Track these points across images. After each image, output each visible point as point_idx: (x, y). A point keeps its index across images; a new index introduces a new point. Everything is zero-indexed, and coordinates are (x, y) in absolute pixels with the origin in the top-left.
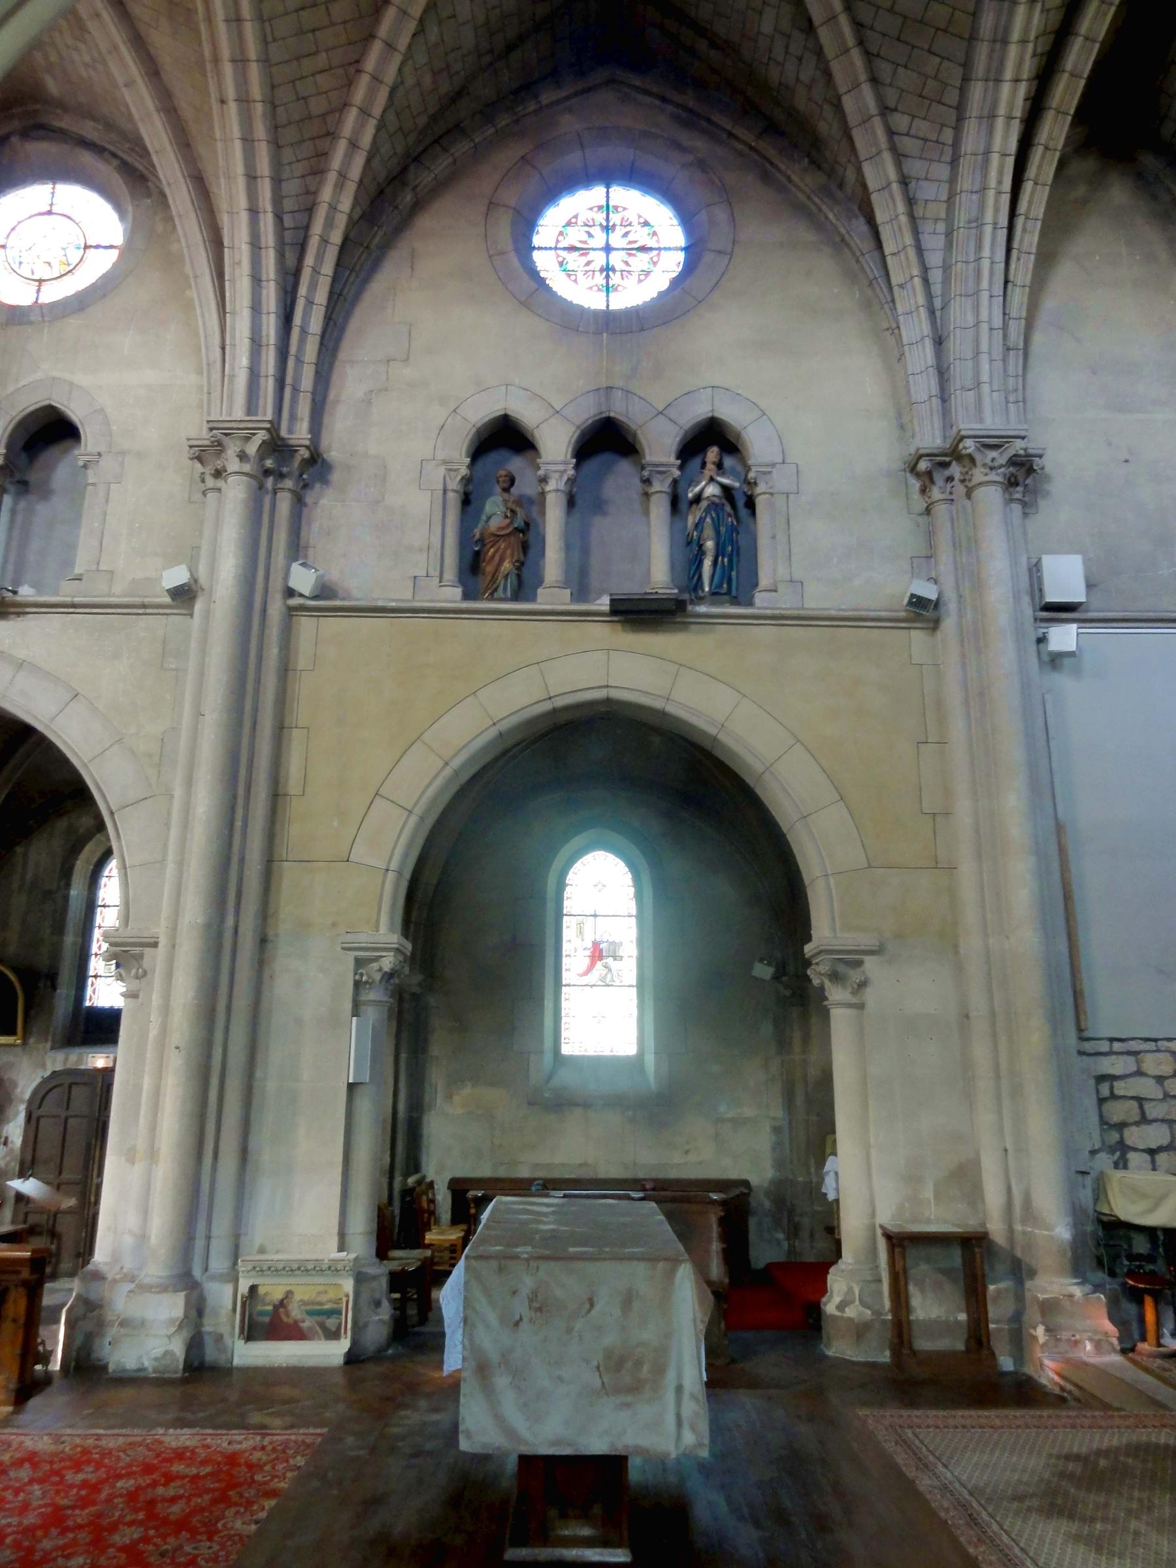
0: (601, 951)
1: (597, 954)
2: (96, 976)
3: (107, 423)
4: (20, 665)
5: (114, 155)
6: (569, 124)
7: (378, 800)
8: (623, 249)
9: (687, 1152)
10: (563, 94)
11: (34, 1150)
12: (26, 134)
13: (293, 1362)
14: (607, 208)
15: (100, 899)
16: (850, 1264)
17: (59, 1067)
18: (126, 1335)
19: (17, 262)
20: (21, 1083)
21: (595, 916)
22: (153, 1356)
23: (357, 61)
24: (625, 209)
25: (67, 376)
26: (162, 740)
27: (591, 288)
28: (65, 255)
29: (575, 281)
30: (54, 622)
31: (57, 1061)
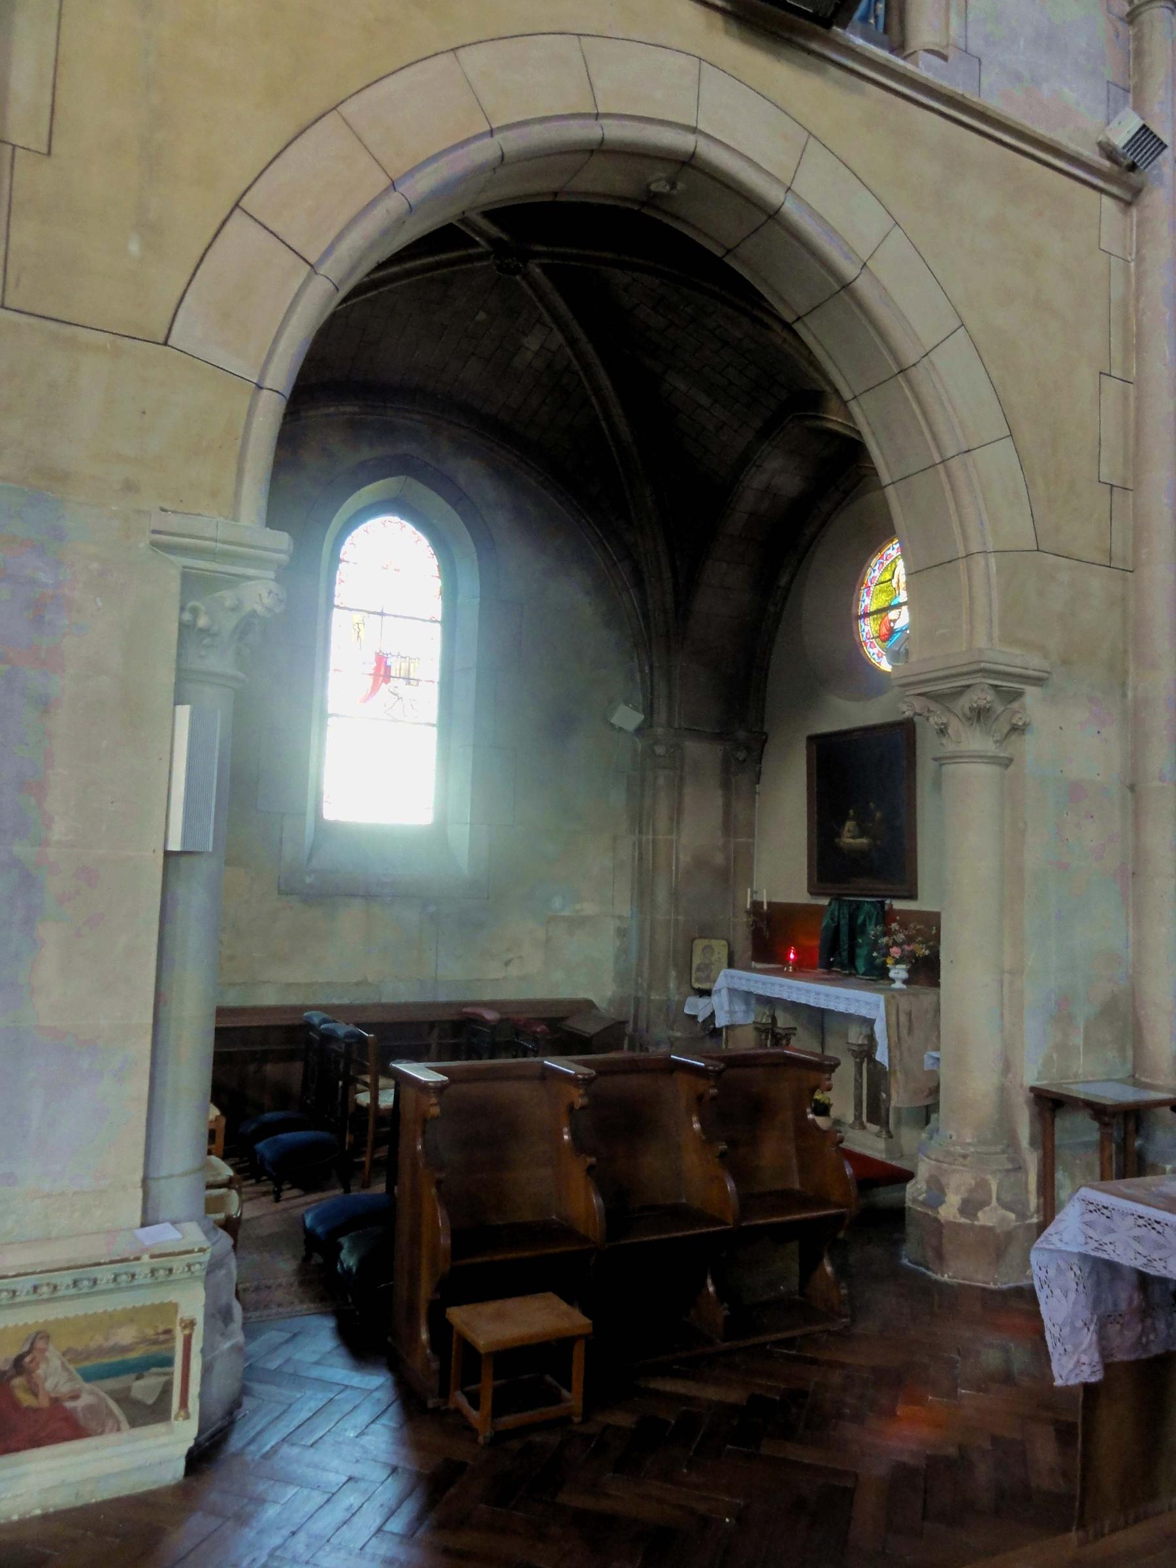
0: (388, 668)
1: (382, 672)
9: (507, 964)
13: (61, 1500)
16: (969, 1144)
21: (382, 614)
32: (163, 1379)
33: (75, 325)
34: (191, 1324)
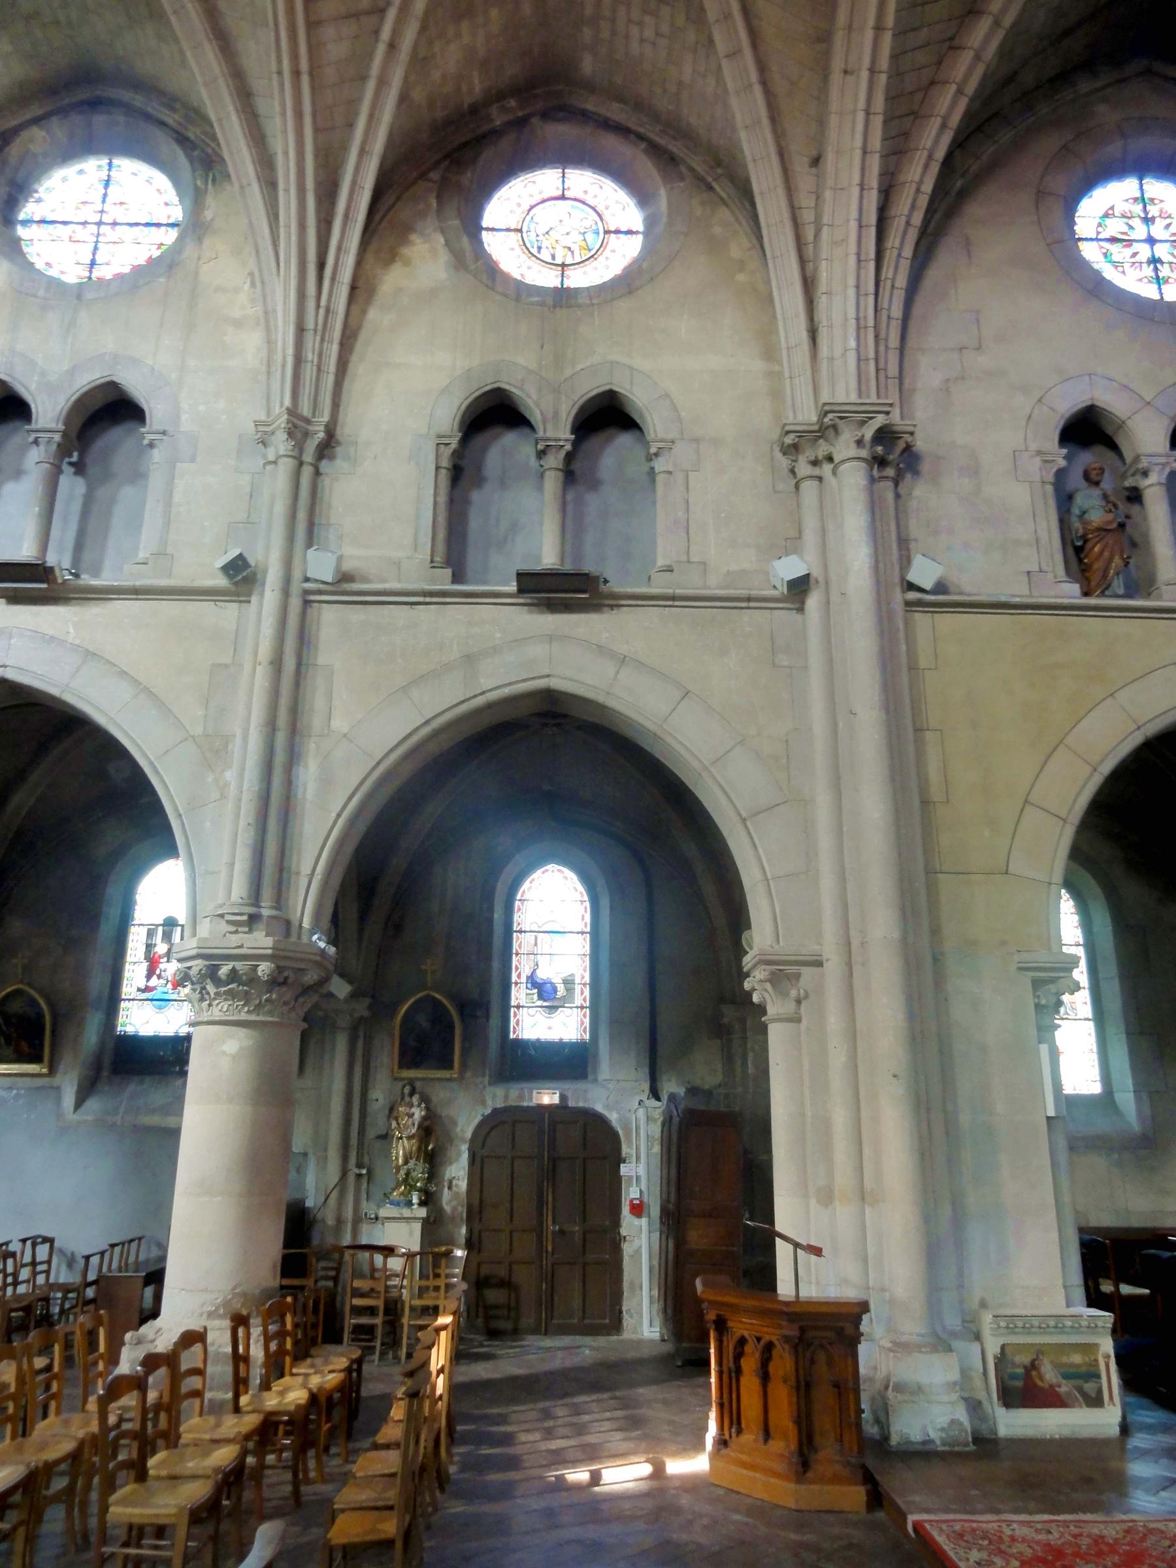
2: (518, 1007)
3: (675, 409)
4: (623, 660)
5: (641, 137)
6: (1106, 114)
7: (1029, 809)
8: (1166, 241)
10: (1099, 84)
11: (481, 1192)
12: (546, 115)
13: (1066, 1432)
14: (1142, 200)
15: (515, 925)
17: (500, 1104)
18: (906, 1402)
19: (535, 246)
20: (461, 1121)
22: (939, 1426)
23: (951, 39)
24: (1161, 201)
25: (624, 360)
26: (787, 741)
27: (1140, 280)
28: (585, 240)
29: (1123, 272)
30: (651, 615)
31: (498, 1097)
32: (1098, 1385)
33: (1038, 776)
34: (1108, 1357)
